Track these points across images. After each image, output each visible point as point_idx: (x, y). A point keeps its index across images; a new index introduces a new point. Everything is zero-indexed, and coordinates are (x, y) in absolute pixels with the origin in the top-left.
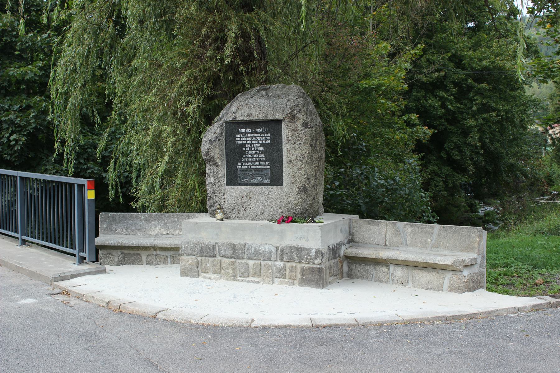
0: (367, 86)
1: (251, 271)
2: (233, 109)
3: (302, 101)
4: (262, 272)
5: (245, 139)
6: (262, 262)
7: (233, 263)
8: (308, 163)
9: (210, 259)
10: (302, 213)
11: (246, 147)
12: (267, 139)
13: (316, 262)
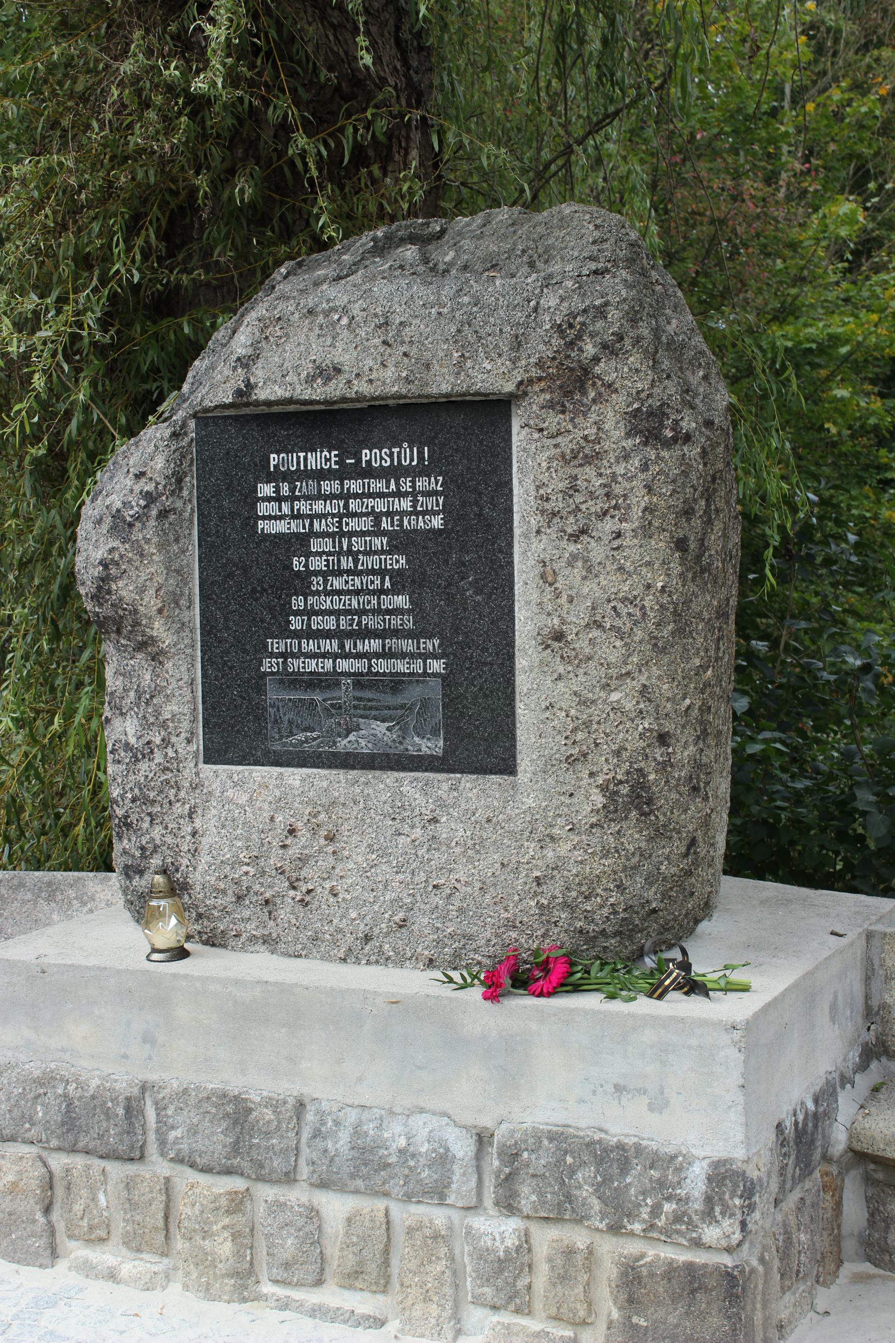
1: (333, 1251)
2: (241, 343)
3: (629, 286)
4: (395, 1262)
5: (302, 506)
6: (397, 1211)
7: (237, 1203)
8: (660, 649)
9: (115, 1170)
10: (627, 930)
11: (308, 554)
13: (711, 1234)
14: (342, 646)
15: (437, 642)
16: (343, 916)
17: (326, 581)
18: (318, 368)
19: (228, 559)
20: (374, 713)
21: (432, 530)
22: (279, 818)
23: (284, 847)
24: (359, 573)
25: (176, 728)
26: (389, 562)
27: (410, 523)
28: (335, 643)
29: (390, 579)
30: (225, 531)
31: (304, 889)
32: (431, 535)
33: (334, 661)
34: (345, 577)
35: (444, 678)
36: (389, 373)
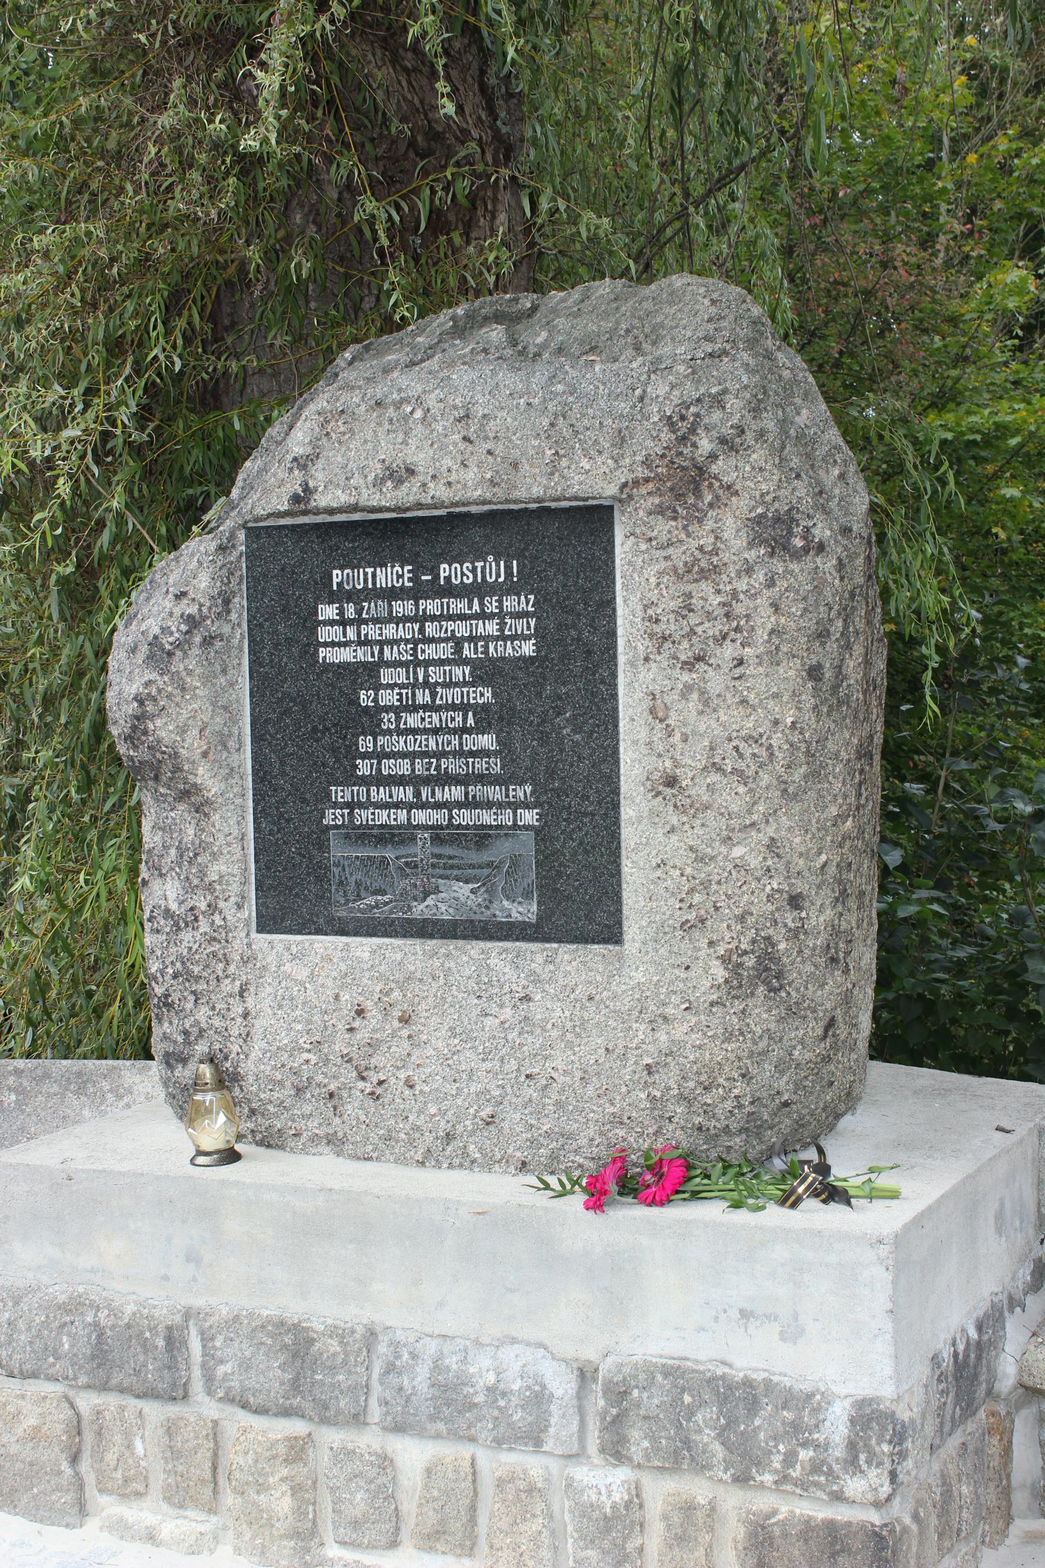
0: (949, 436)
1: (409, 1506)
2: (298, 442)
4: (483, 1521)
5: (371, 631)
6: (485, 1459)
7: (297, 1450)
9: (155, 1411)
11: (377, 687)
13: (854, 1486)
14: (417, 794)
15: (529, 789)
16: (420, 1112)
17: (398, 718)
19: (284, 693)
20: (455, 872)
21: (523, 658)
22: (345, 997)
24: (437, 709)
25: (224, 891)
26: (472, 695)
27: (496, 650)
28: (410, 791)
30: (281, 660)
32: (521, 664)
33: (409, 812)
34: (421, 713)
35: (537, 831)
36: (471, 475)
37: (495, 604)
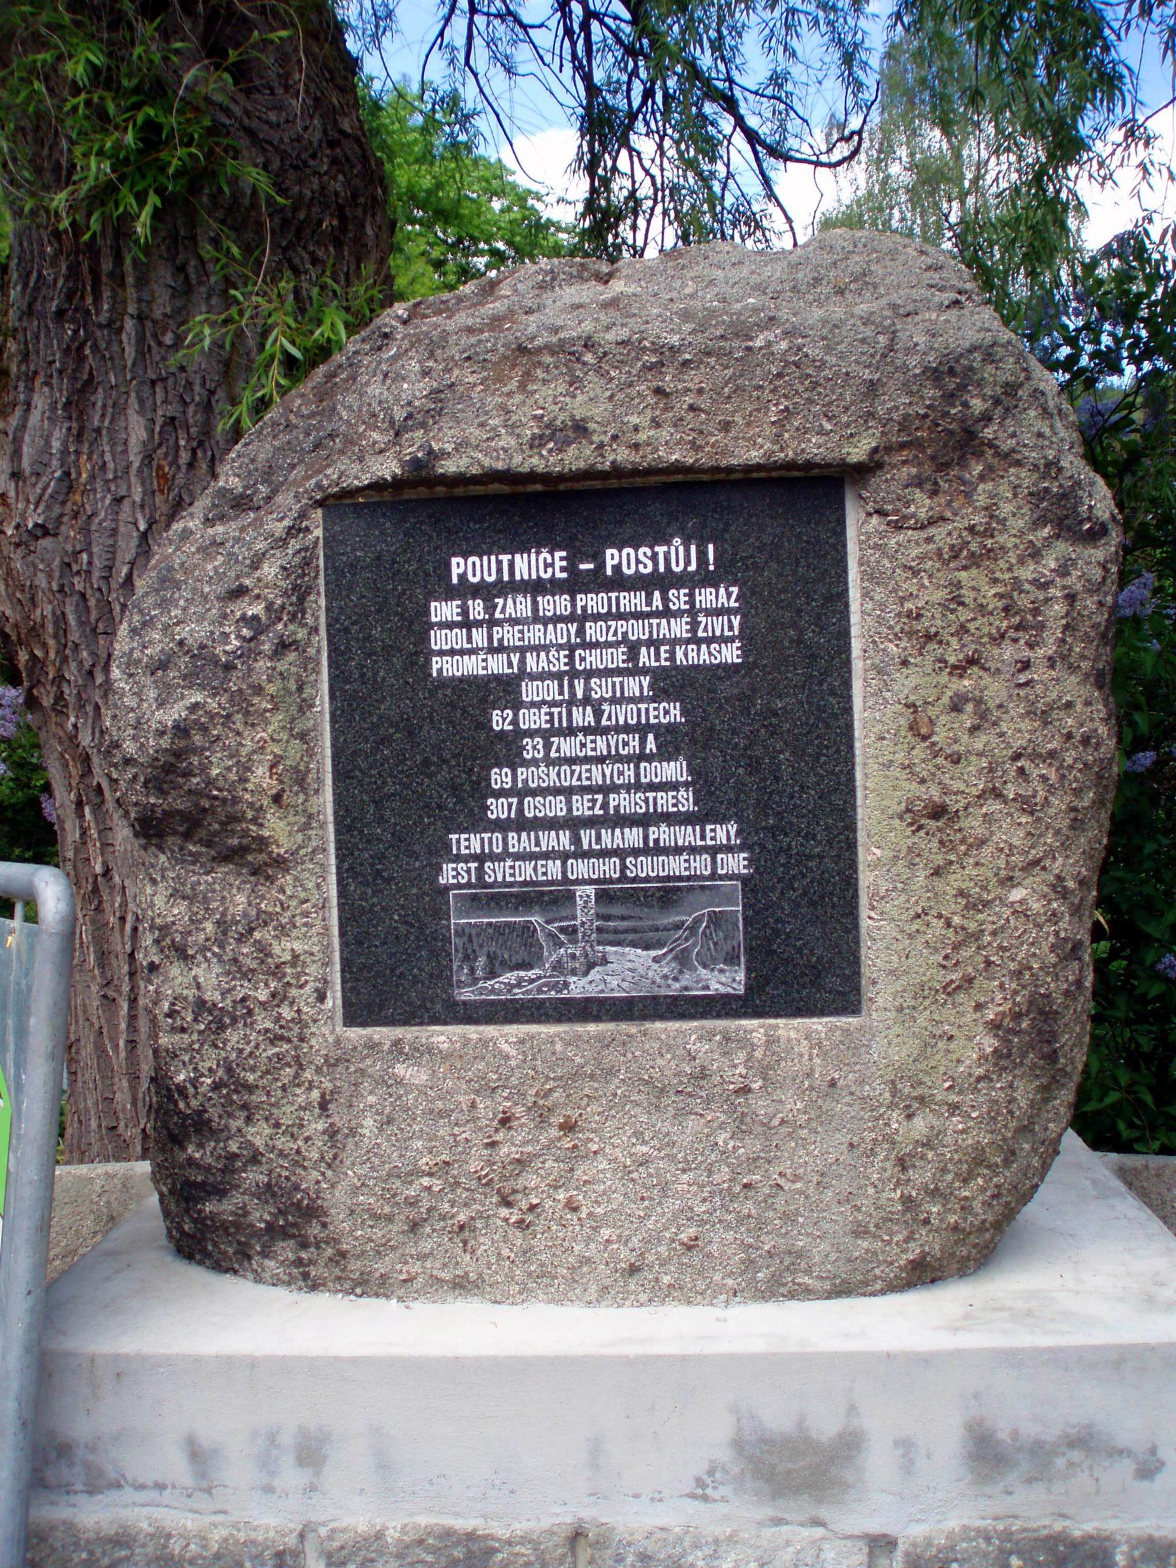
11: (517, 705)
12: (711, 630)
14: (576, 840)
15: (733, 828)
16: (588, 1240)
17: (548, 746)
18: (547, 427)
19: (380, 717)
20: (630, 937)
21: (723, 666)
23: (493, 1144)
24: (605, 731)
25: (297, 976)
26: (652, 713)
27: (686, 655)
28: (565, 838)
29: (656, 739)
30: (376, 674)
31: (524, 1205)
32: (720, 672)
33: (564, 864)
34: (580, 736)
35: (745, 880)
37: (683, 599)
